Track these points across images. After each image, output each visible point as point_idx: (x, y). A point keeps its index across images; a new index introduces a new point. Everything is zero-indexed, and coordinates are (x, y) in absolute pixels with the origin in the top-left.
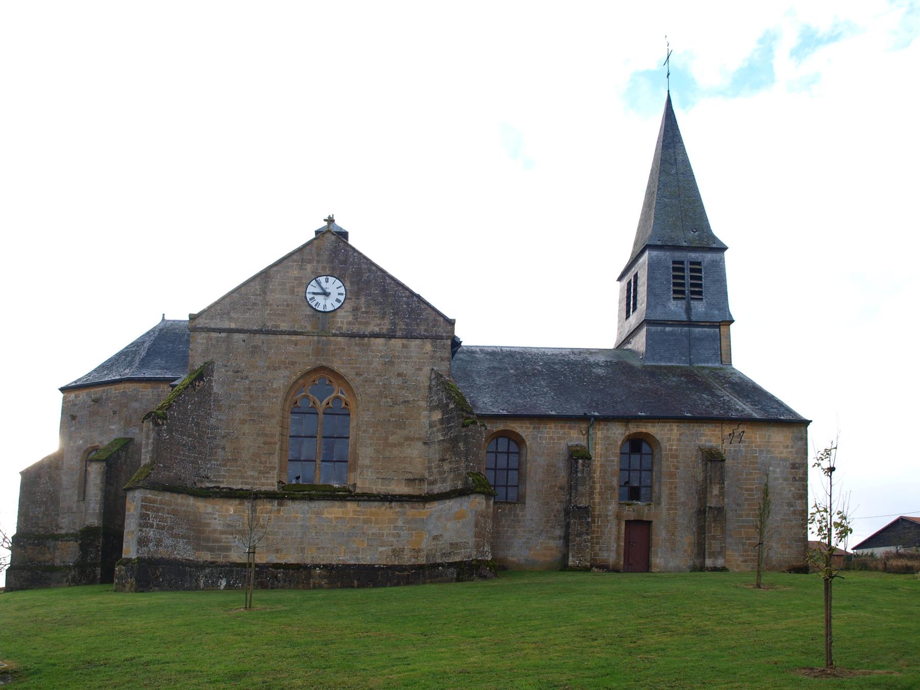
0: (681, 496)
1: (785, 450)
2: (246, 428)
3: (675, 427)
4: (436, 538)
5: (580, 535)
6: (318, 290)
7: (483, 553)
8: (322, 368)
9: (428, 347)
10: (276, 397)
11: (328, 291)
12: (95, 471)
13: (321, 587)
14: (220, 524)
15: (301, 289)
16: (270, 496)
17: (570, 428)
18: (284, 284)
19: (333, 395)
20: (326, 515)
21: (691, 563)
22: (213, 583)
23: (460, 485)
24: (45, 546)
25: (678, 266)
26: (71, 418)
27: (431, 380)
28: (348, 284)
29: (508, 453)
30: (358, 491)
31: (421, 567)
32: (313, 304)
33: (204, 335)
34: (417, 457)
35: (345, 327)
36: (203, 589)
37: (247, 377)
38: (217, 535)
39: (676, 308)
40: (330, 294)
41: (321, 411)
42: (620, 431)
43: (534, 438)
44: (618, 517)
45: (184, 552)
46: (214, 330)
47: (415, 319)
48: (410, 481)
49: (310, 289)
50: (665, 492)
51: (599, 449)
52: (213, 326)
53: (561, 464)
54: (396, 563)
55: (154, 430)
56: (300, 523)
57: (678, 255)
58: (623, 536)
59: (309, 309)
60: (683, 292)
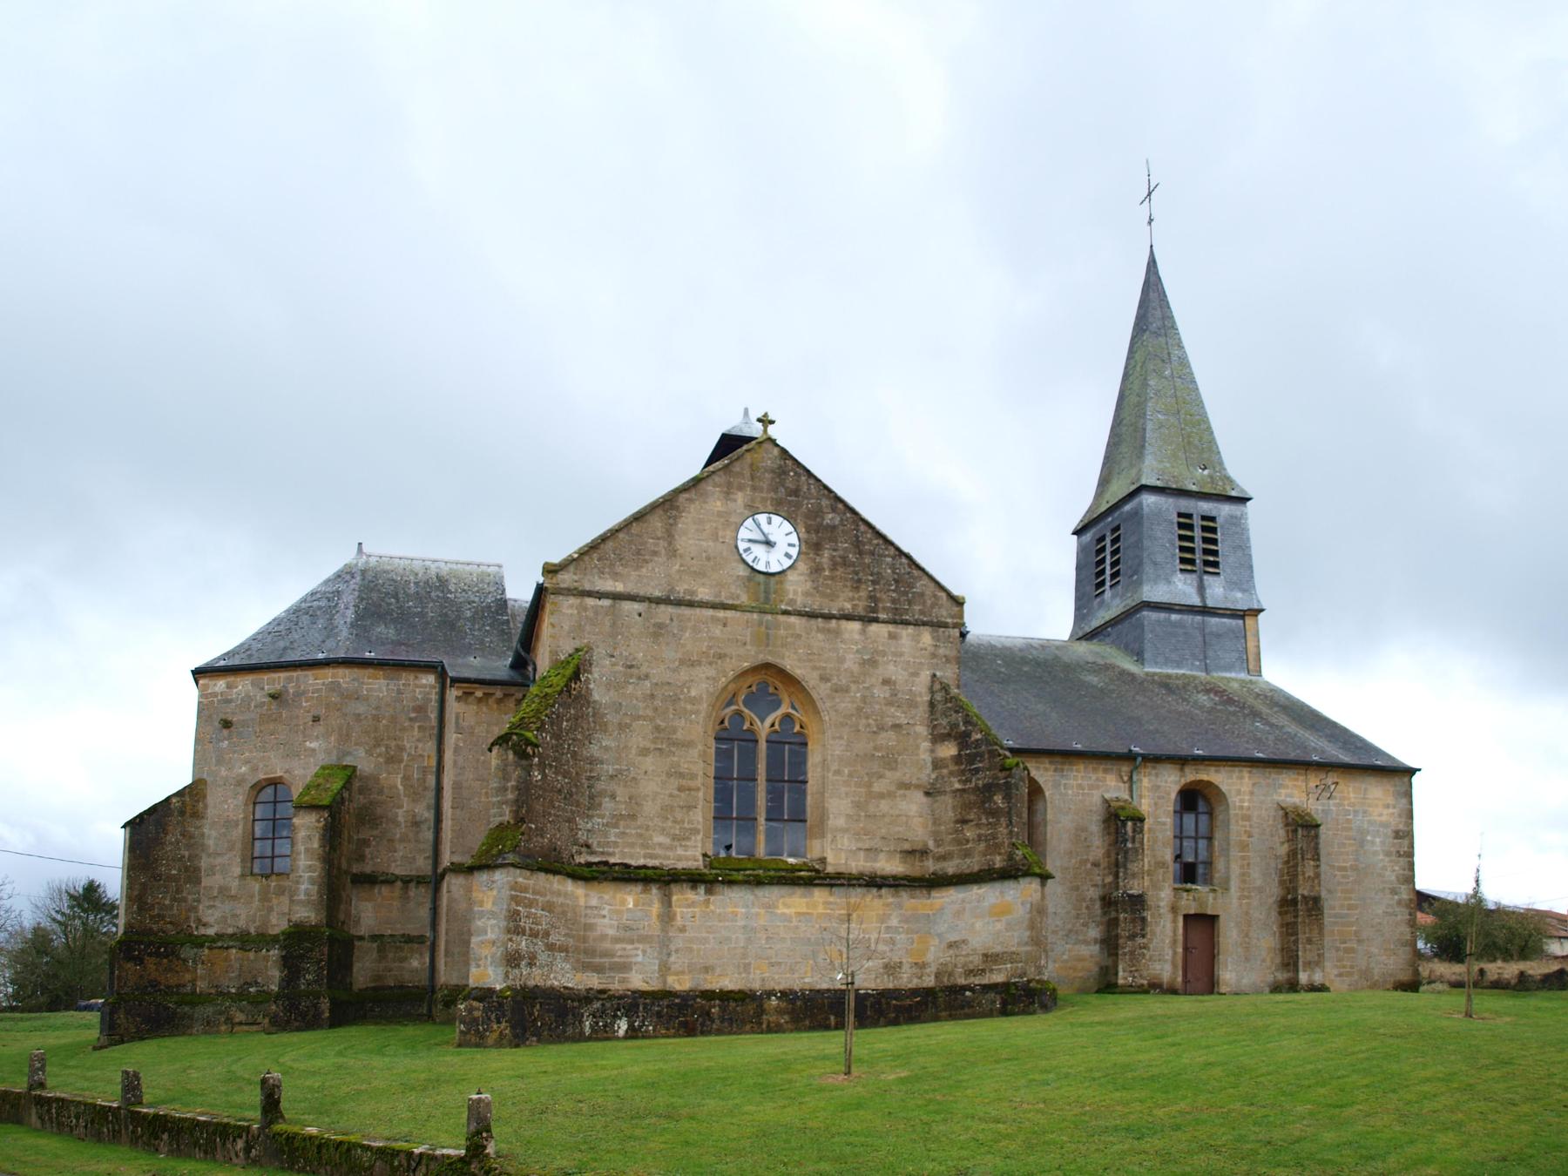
0: (1256, 876)
1: (1386, 812)
2: (649, 762)
3: (1245, 772)
5: (1132, 937)
6: (757, 536)
8: (767, 666)
9: (926, 637)
10: (697, 712)
11: (772, 538)
14: (611, 926)
15: (729, 534)
16: (693, 879)
17: (1106, 771)
18: (701, 522)
20: (781, 910)
21: (1270, 978)
22: (605, 1026)
23: (998, 862)
24: (178, 958)
26: (216, 725)
27: (932, 692)
30: (830, 869)
31: (929, 992)
32: (749, 559)
33: (572, 600)
34: (913, 817)
35: (799, 600)
36: (589, 1039)
37: (647, 676)
38: (607, 945)
40: (773, 543)
42: (1172, 778)
44: (1174, 909)
45: (565, 976)
46: (590, 594)
47: (906, 593)
49: (743, 533)
50: (1235, 869)
52: (588, 587)
53: (1095, 828)
54: (891, 986)
55: (517, 765)
56: (741, 923)
57: (1186, 505)
58: (1180, 938)
59: (742, 566)
60: (1192, 562)
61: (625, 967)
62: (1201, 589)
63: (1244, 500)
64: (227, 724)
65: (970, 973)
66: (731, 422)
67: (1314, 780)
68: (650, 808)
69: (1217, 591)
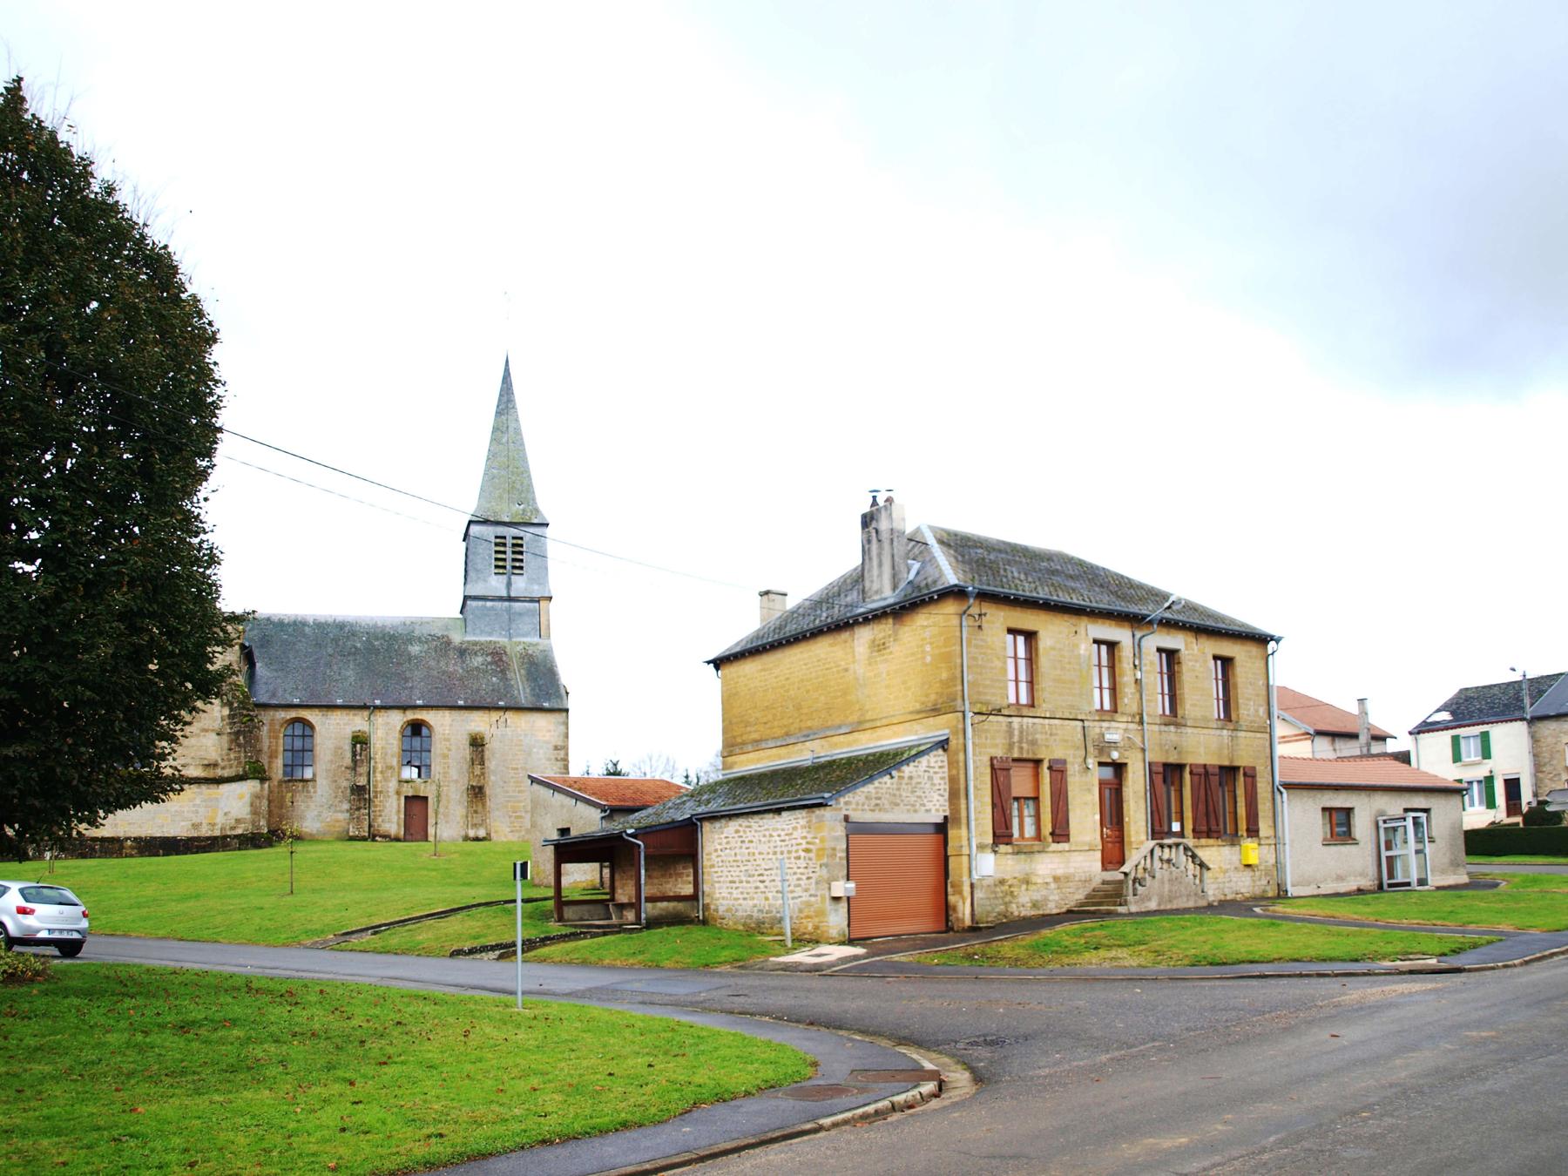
7: (259, 827)
13: (132, 856)
25: (500, 541)
39: (495, 584)
51: (380, 733)
53: (348, 748)
57: (501, 530)
62: (509, 584)
65: (233, 828)
67: (495, 715)
69: (520, 585)
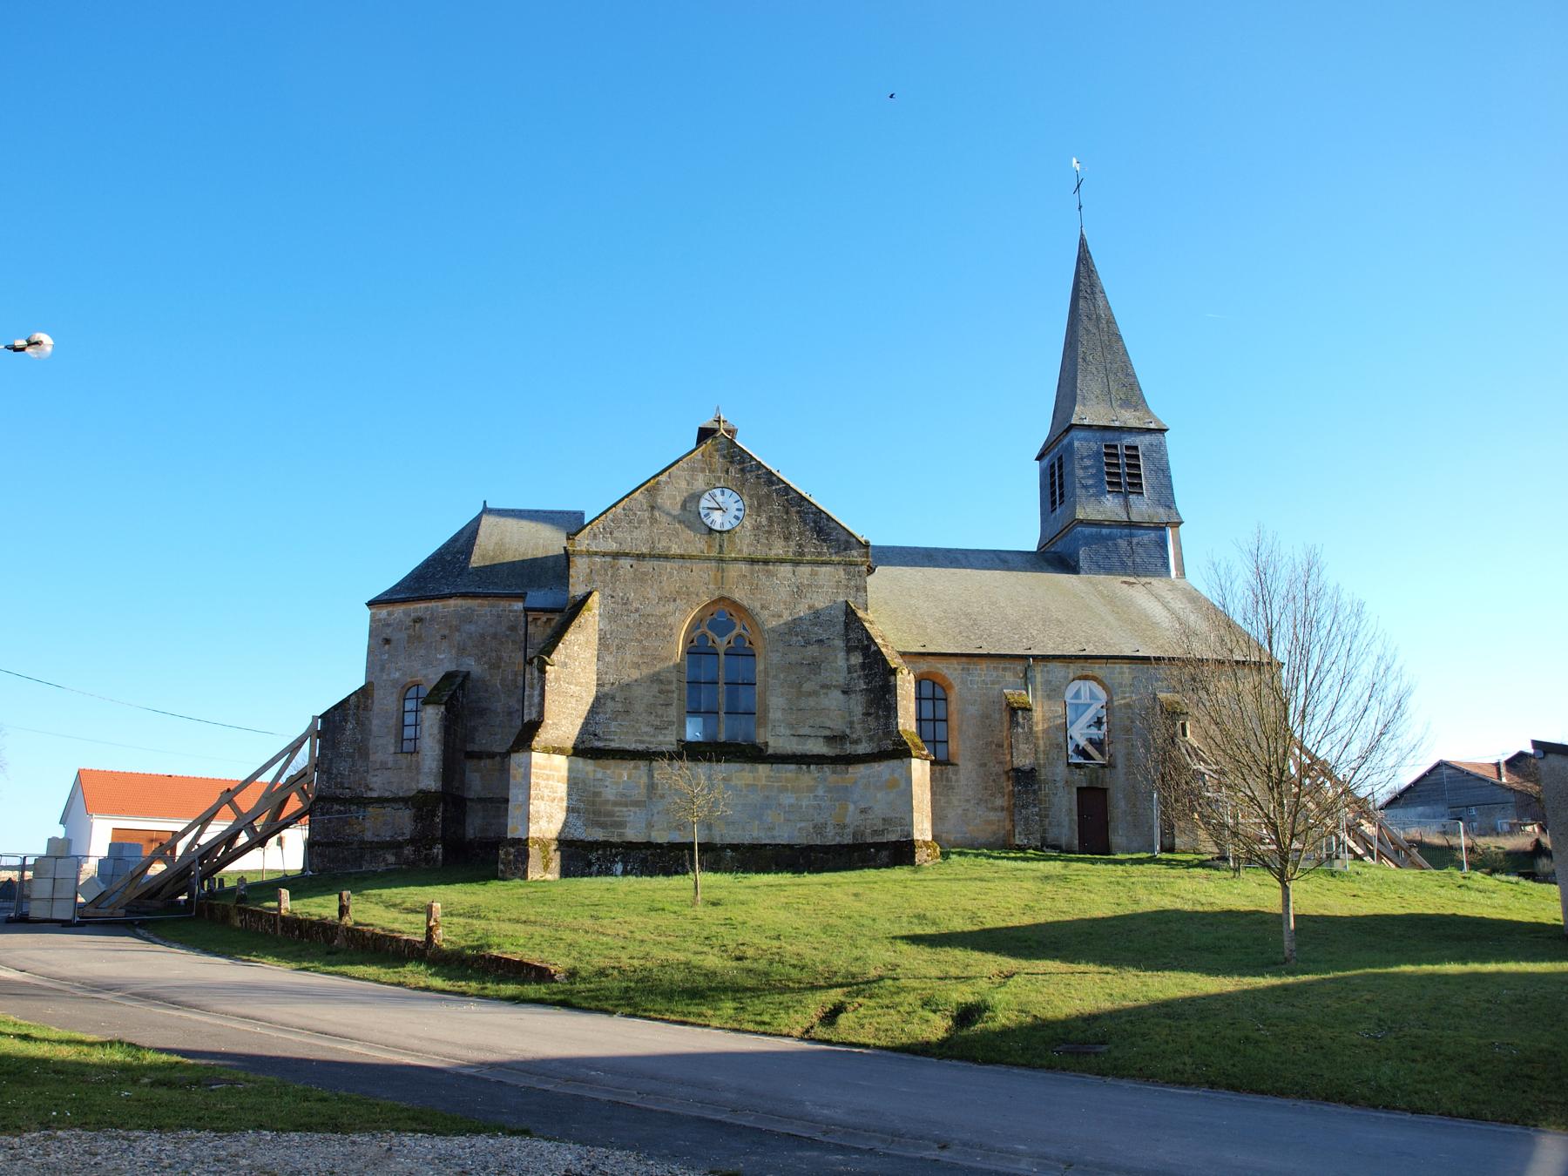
4: (863, 811)
8: (722, 599)
12: (432, 716)
19: (735, 632)
28: (745, 498)
29: (934, 699)
38: (609, 808)
41: (721, 651)
43: (963, 682)
48: (830, 739)
61: (622, 825)
62: (1127, 506)
63: (1162, 431)
64: (387, 641)
65: (875, 832)
66: (707, 422)
68: (639, 707)
